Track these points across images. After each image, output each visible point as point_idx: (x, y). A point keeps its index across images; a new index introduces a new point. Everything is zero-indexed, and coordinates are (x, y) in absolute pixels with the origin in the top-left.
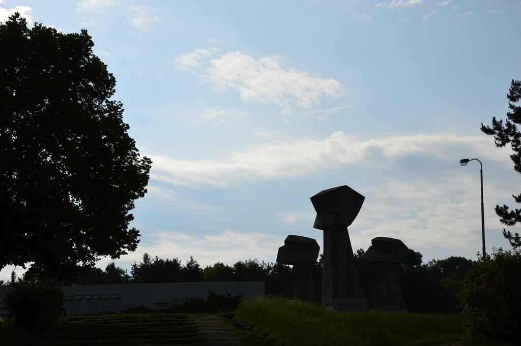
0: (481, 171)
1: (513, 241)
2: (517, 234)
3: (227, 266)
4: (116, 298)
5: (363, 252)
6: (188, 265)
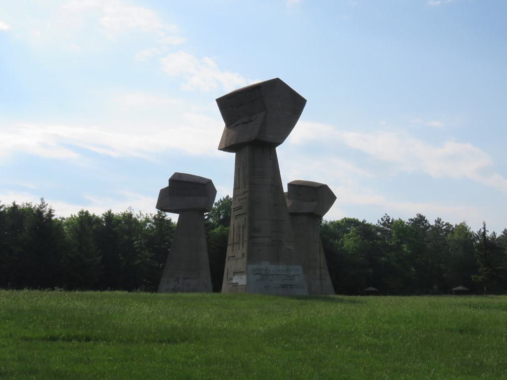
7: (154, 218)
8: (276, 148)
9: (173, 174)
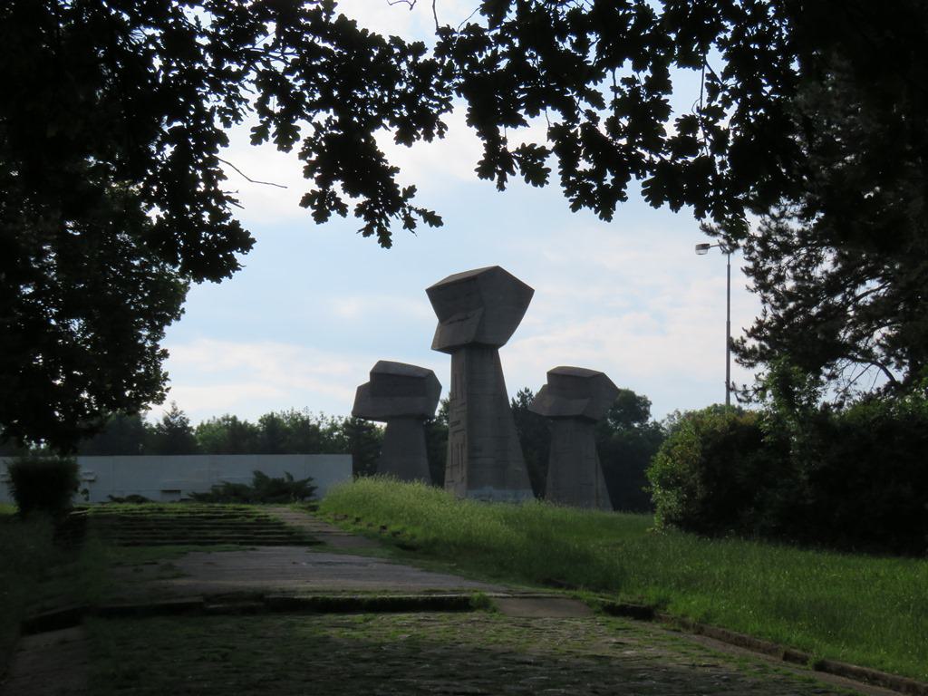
0: (729, 266)
1: (740, 396)
2: (745, 386)
3: (246, 423)
4: (90, 481)
5: (530, 395)
6: (167, 421)
7: (346, 424)
8: (499, 350)
9: (375, 363)
